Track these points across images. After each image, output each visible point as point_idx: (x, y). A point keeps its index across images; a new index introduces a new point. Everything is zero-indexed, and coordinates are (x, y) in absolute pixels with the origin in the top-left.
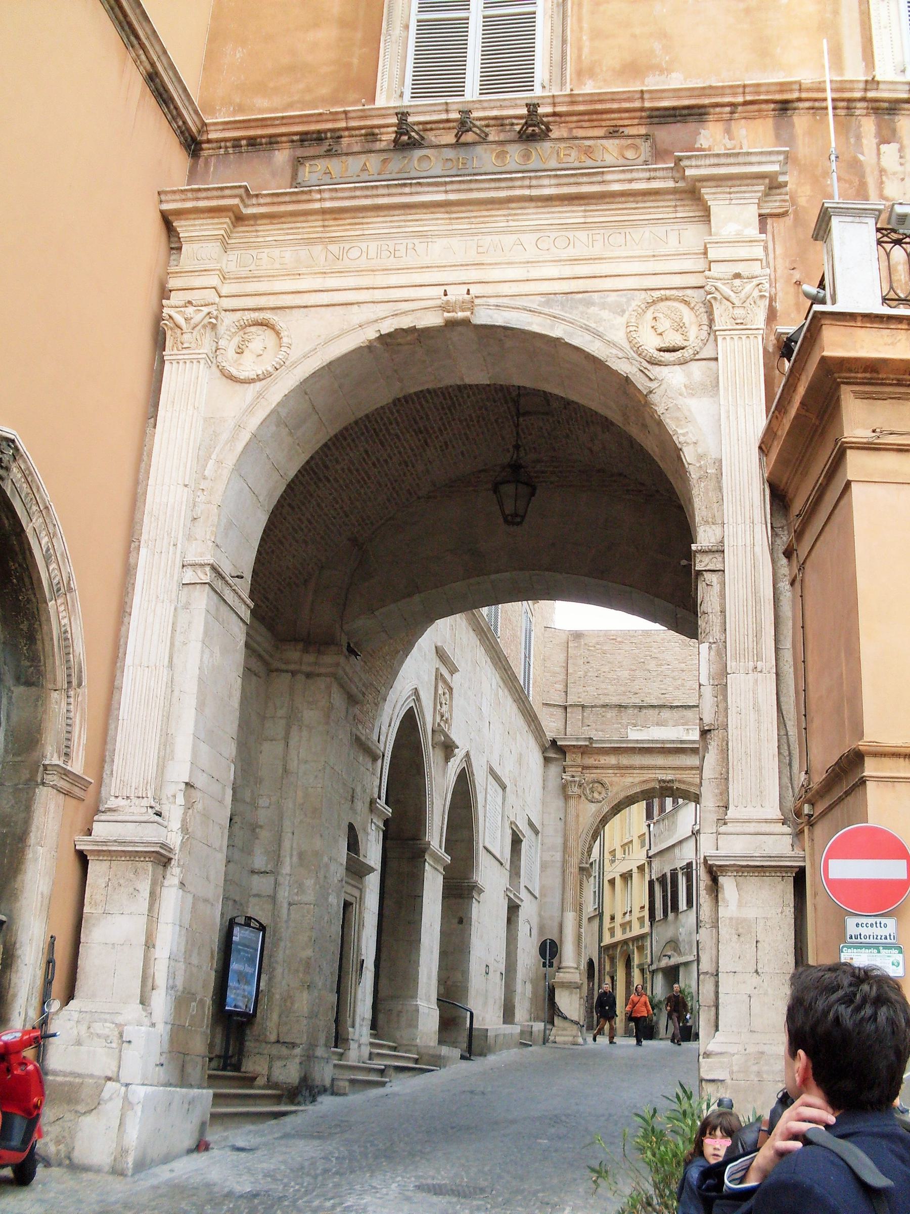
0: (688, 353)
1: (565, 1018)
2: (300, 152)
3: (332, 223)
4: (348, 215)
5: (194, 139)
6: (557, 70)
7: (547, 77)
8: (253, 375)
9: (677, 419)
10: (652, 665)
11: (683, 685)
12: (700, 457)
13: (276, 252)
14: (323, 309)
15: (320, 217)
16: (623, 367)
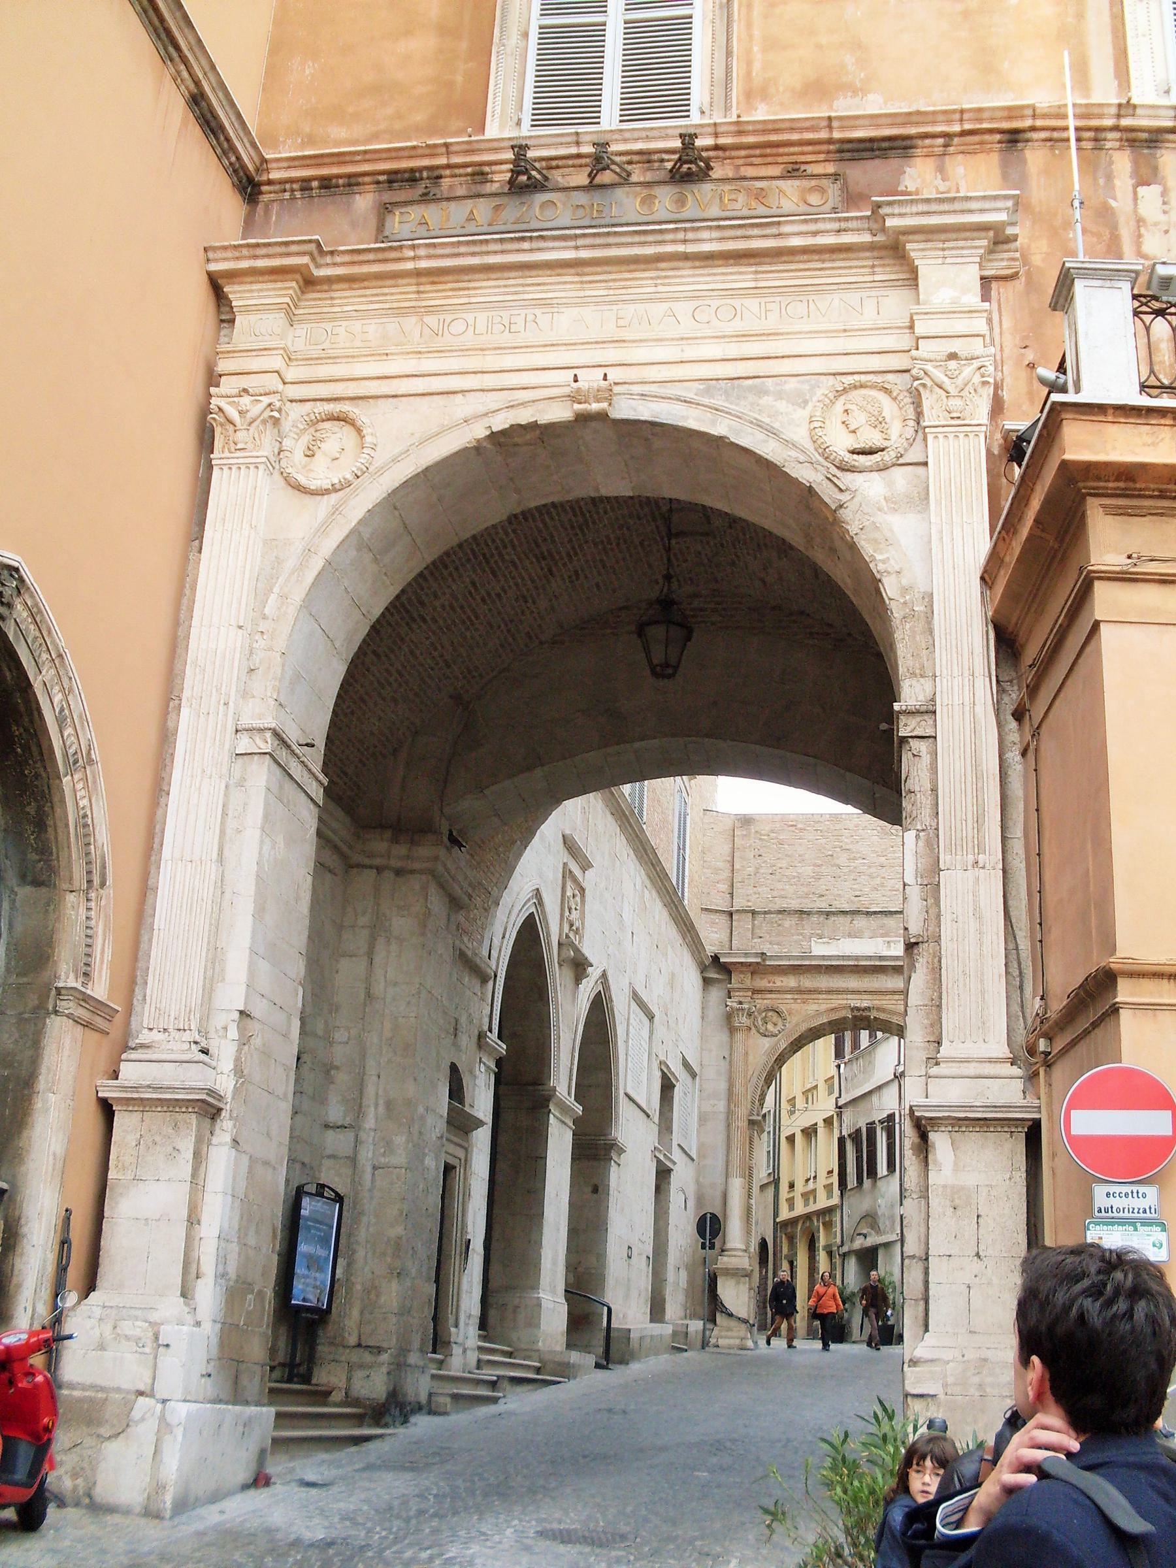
0: (889, 456)
1: (731, 1315)
2: (387, 197)
3: (428, 288)
4: (450, 278)
5: (250, 180)
6: (719, 91)
7: (707, 99)
8: (326, 485)
9: (876, 541)
10: (842, 859)
11: (882, 885)
12: (905, 590)
13: (357, 326)
14: (418, 399)
15: (413, 281)
16: (805, 475)
